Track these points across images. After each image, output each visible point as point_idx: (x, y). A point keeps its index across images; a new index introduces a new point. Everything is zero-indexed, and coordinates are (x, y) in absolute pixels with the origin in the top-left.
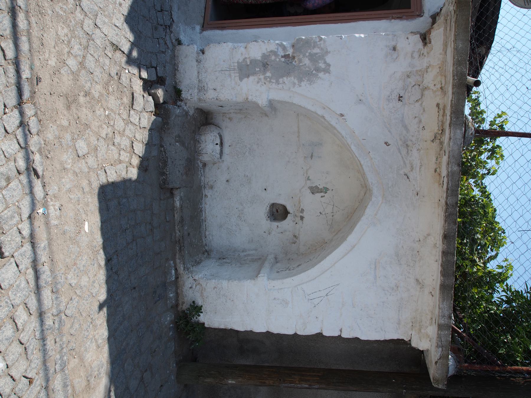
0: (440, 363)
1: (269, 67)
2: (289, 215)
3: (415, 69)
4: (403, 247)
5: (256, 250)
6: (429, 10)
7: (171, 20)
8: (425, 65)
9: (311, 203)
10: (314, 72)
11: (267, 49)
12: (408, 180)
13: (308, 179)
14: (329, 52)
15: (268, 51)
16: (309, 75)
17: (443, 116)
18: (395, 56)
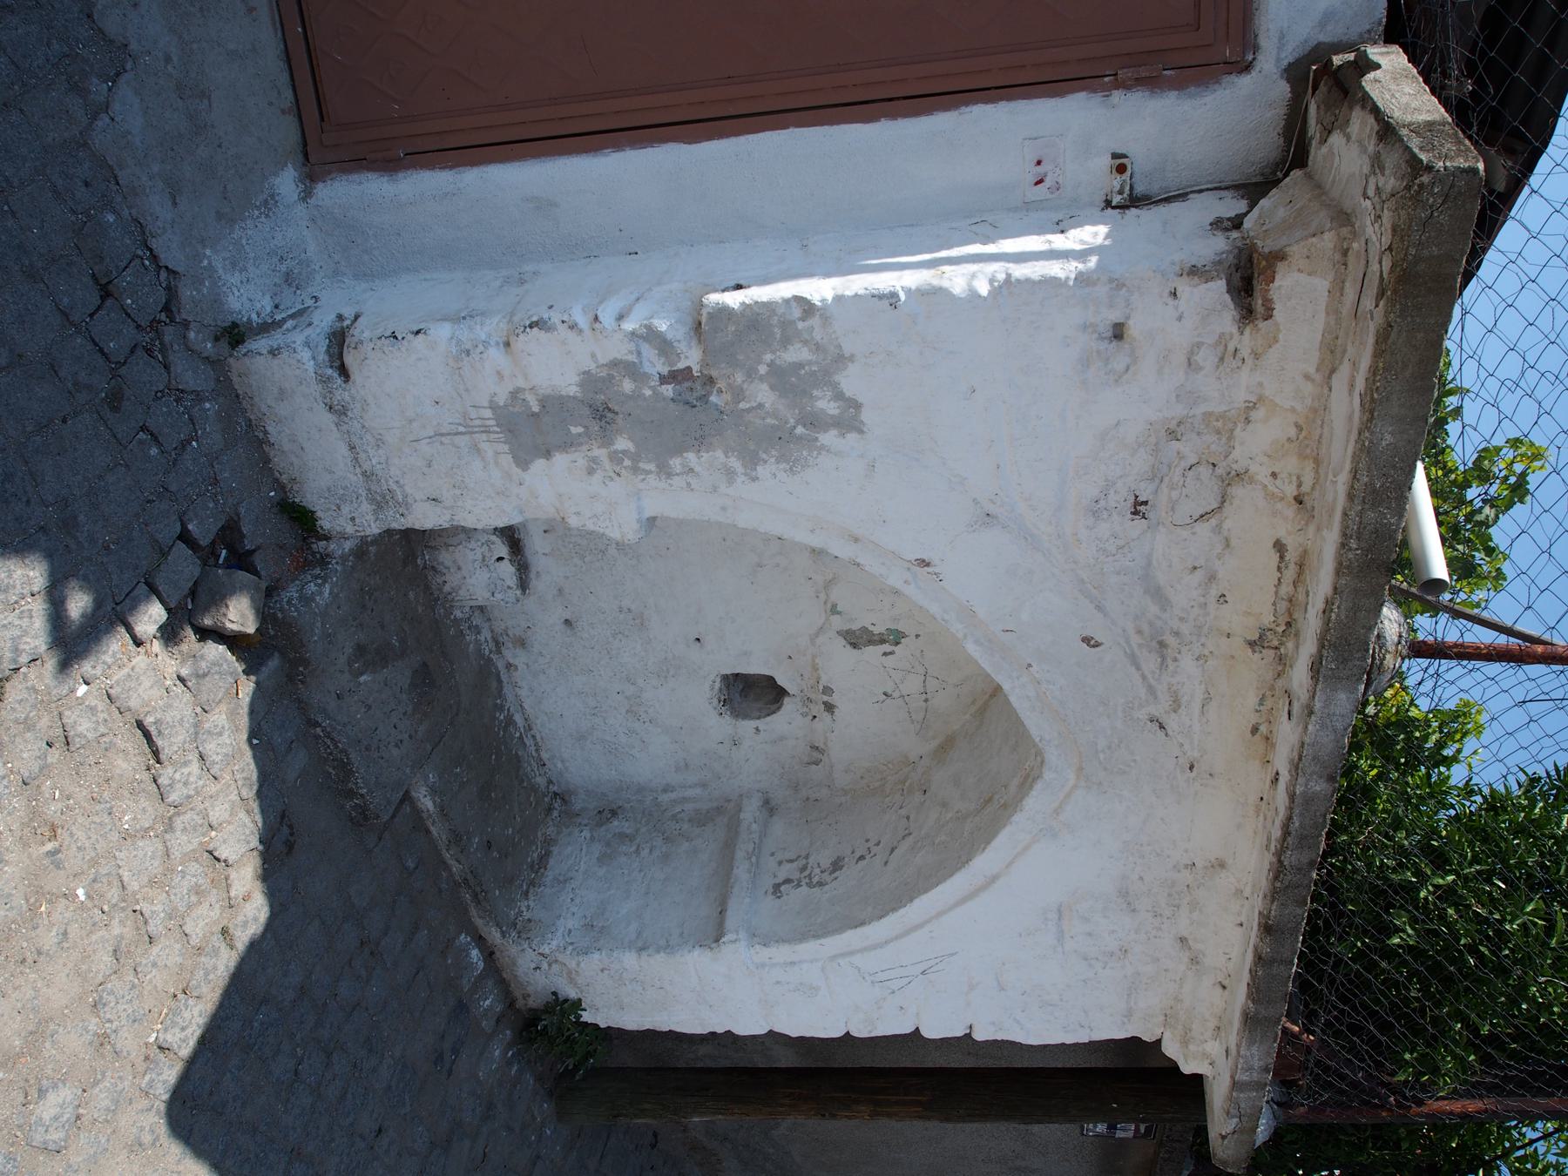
0: (1234, 1118)
1: (620, 419)
2: (786, 700)
3: (1199, 410)
4: (1141, 878)
5: (704, 785)
6: (1282, 37)
7: (163, 275)
8: (1241, 396)
9: (847, 671)
10: (800, 430)
11: (593, 356)
12: (1161, 734)
13: (834, 610)
14: (852, 358)
15: (602, 361)
16: (788, 440)
17: (1295, 584)
18: (1119, 363)
